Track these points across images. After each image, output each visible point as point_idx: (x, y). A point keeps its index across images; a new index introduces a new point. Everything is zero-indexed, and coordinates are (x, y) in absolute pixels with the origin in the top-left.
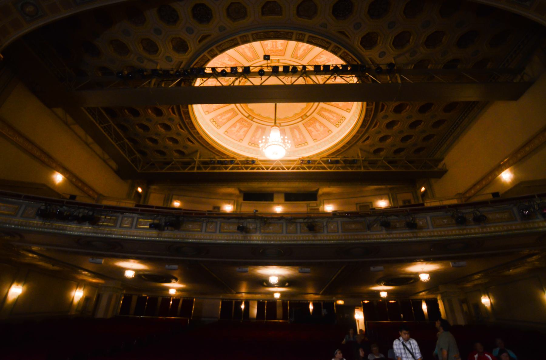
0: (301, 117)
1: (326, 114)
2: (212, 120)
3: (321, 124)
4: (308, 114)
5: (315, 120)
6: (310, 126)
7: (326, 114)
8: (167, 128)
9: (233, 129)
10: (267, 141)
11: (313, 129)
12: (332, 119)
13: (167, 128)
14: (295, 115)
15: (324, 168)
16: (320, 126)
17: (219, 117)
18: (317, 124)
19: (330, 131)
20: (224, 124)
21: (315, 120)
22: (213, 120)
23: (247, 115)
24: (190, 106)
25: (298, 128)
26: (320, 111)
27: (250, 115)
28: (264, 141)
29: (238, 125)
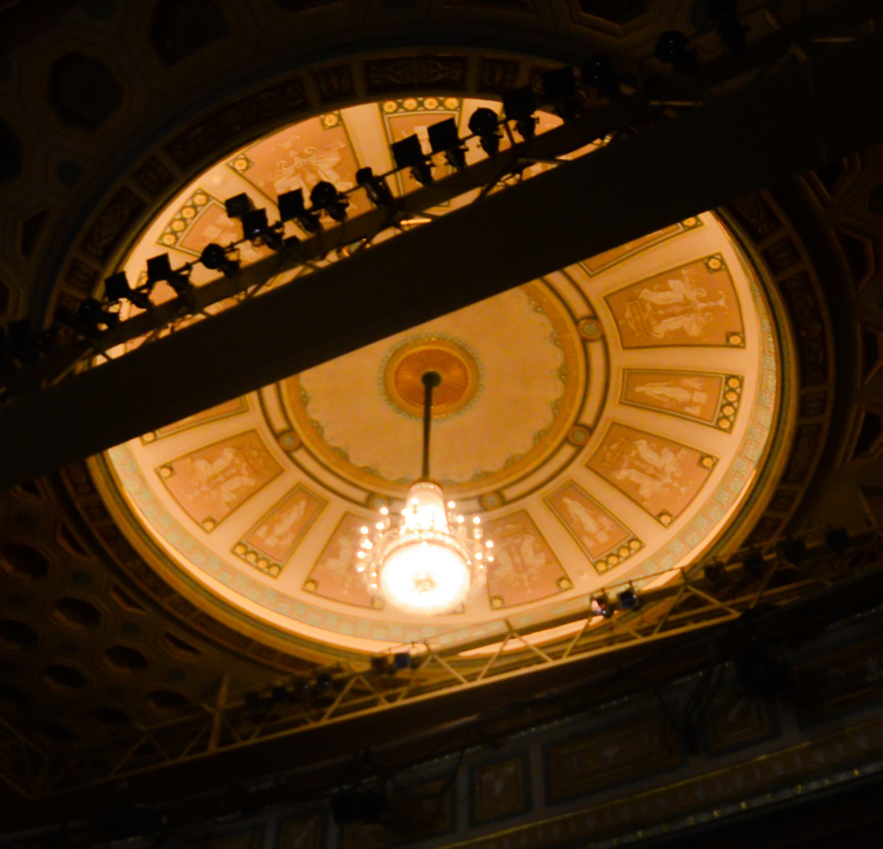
0: (566, 440)
1: (656, 391)
2: (240, 550)
3: (660, 442)
4: (588, 418)
5: (628, 434)
6: (616, 468)
7: (656, 391)
8: (85, 613)
9: (201, 465)
10: (396, 520)
11: (634, 476)
12: (690, 403)
13: (85, 613)
14: (540, 438)
15: (721, 613)
16: (658, 451)
17: (261, 533)
18: (642, 446)
19: (703, 457)
20: (291, 551)
21: (628, 434)
22: (246, 547)
23: (280, 425)
24: (92, 462)
25: (574, 489)
26: (627, 387)
27: (291, 430)
28: (380, 526)
29: (228, 454)
